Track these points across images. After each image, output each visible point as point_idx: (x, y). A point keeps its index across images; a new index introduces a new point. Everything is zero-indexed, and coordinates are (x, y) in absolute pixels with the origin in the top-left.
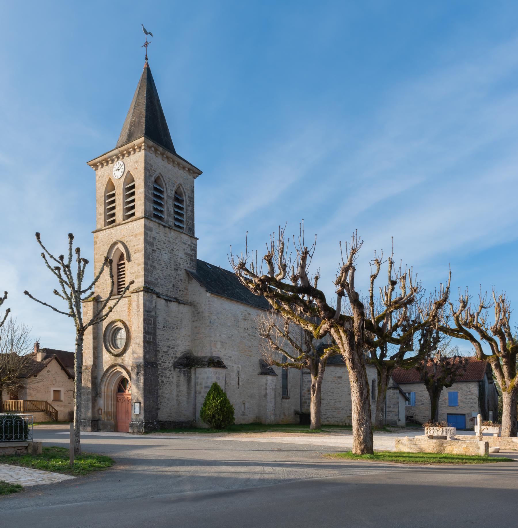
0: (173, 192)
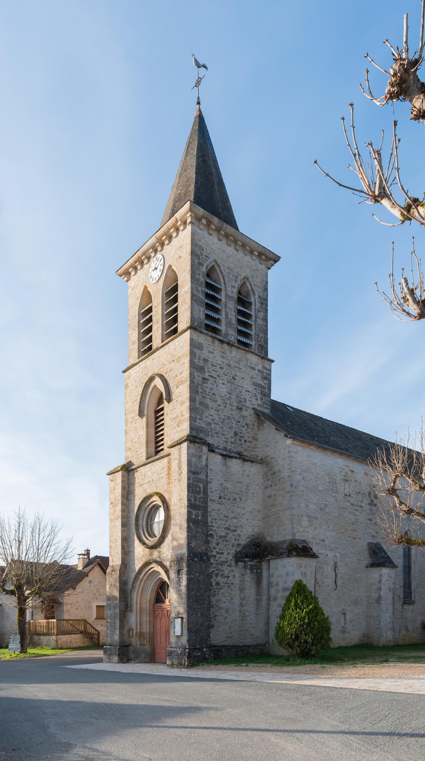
0: (235, 290)
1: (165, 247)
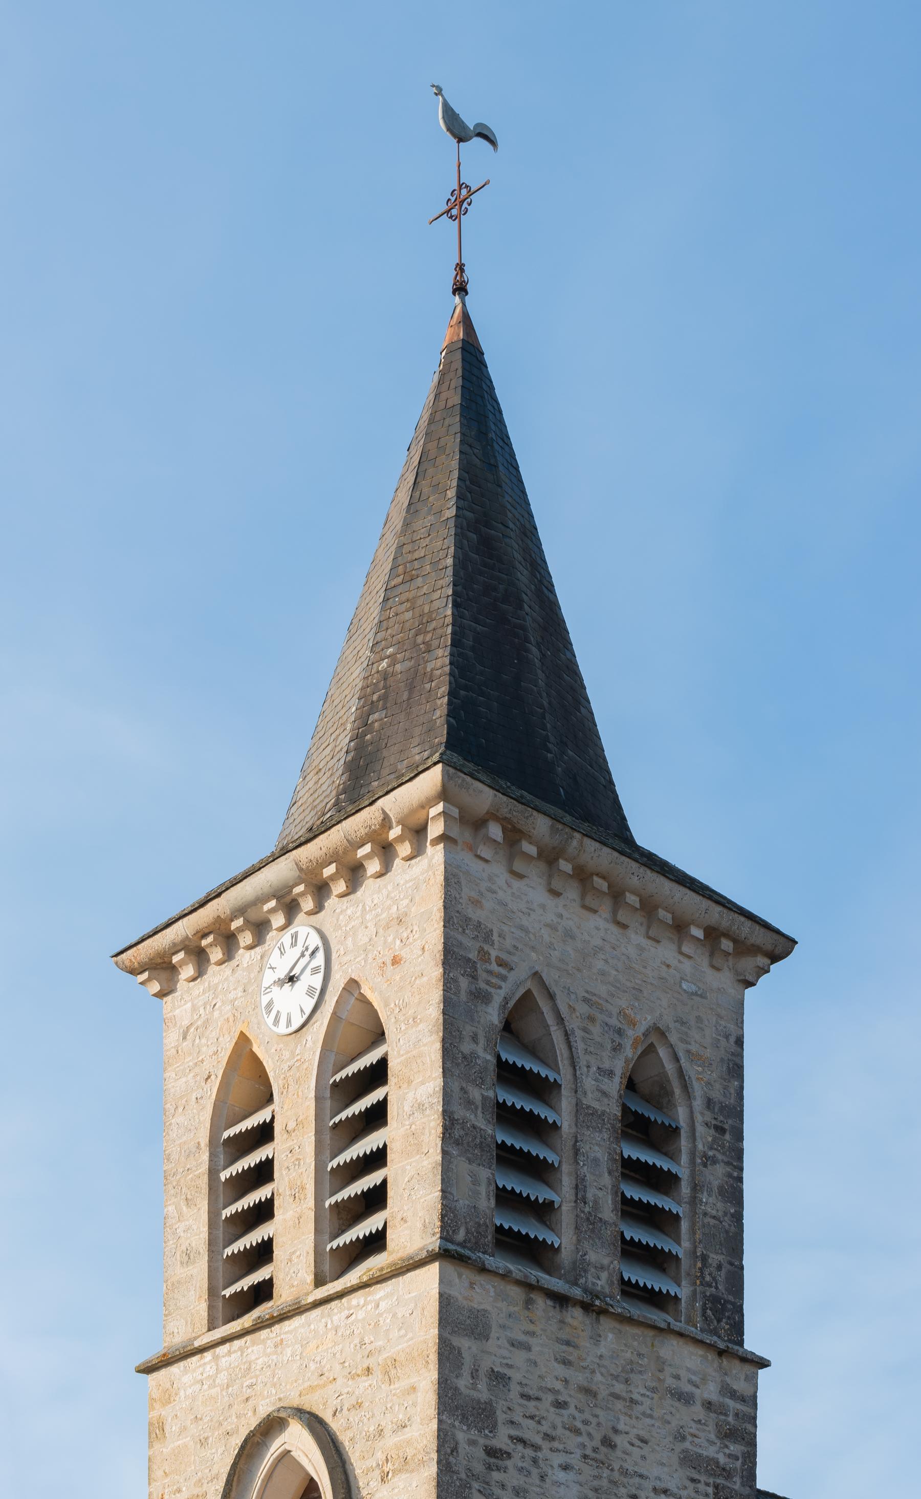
0: (614, 1086)
1: (331, 903)
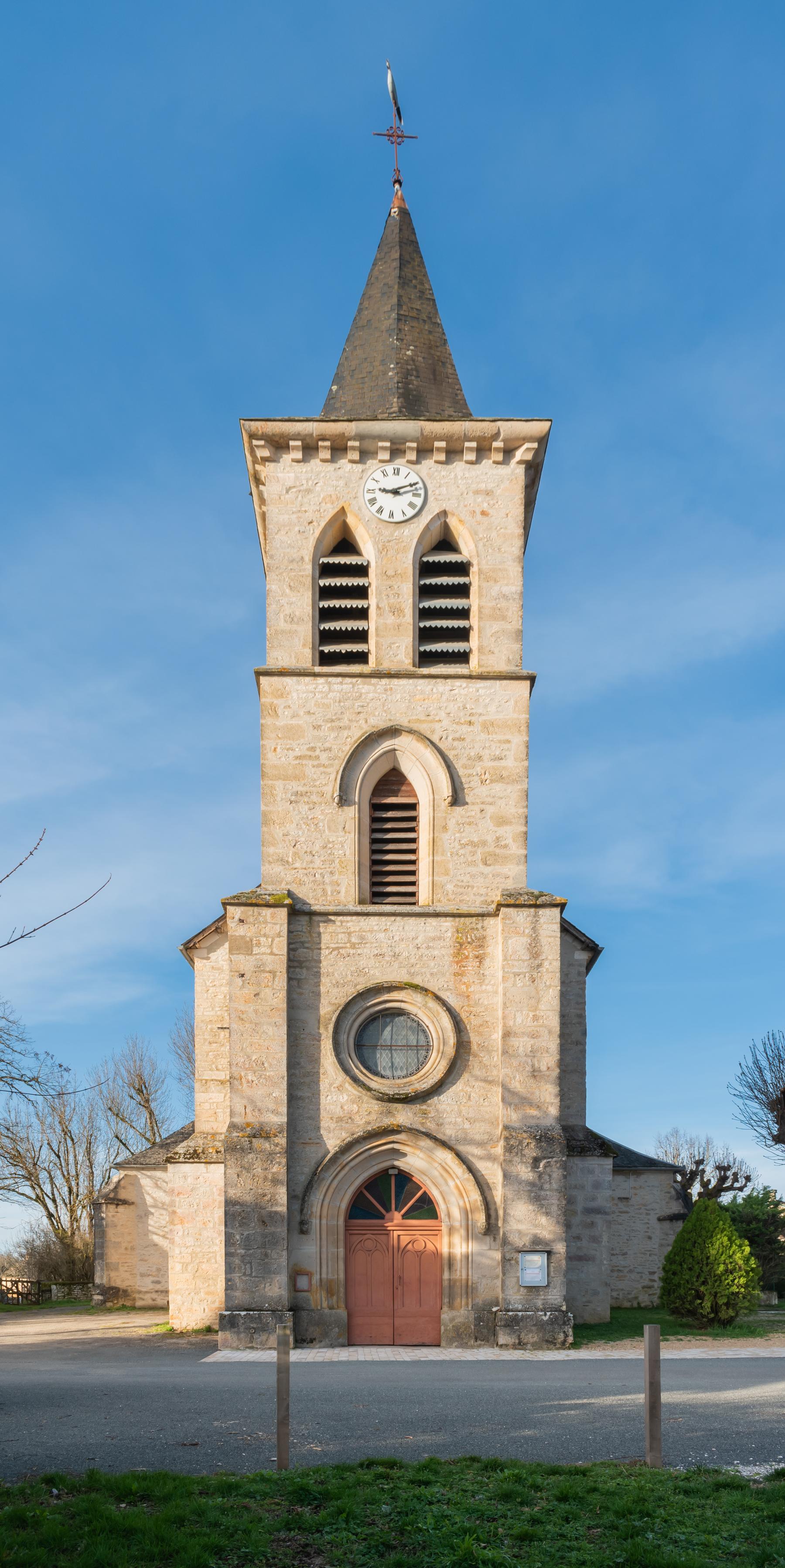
1: (487, 463)
